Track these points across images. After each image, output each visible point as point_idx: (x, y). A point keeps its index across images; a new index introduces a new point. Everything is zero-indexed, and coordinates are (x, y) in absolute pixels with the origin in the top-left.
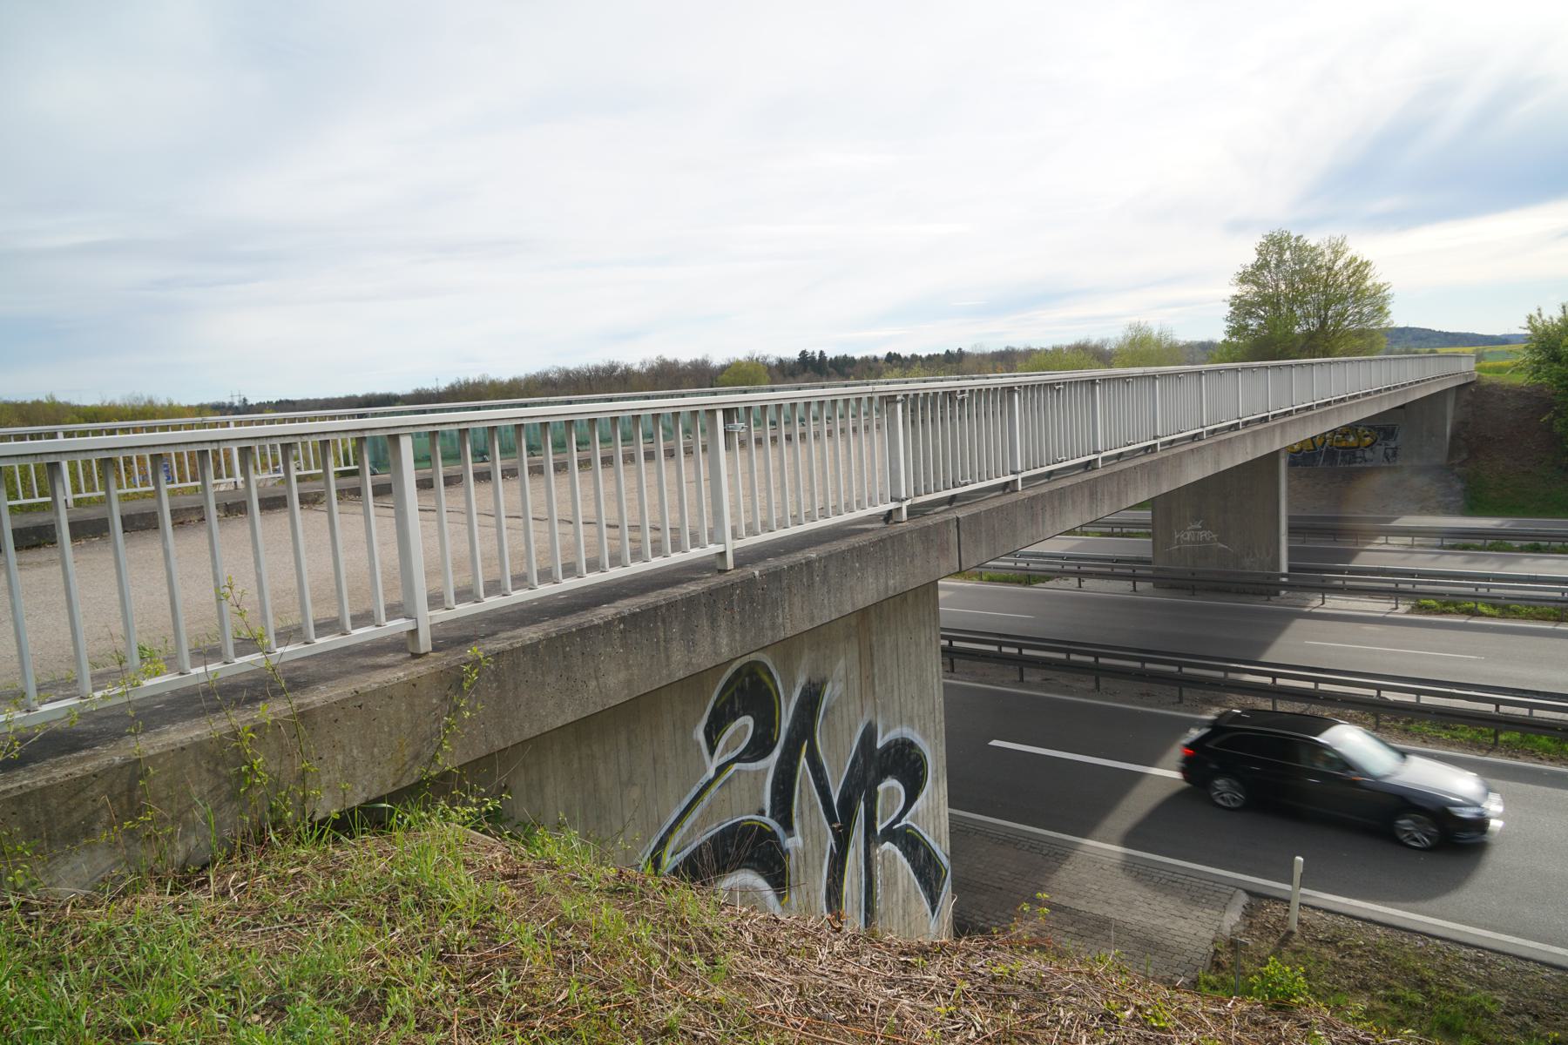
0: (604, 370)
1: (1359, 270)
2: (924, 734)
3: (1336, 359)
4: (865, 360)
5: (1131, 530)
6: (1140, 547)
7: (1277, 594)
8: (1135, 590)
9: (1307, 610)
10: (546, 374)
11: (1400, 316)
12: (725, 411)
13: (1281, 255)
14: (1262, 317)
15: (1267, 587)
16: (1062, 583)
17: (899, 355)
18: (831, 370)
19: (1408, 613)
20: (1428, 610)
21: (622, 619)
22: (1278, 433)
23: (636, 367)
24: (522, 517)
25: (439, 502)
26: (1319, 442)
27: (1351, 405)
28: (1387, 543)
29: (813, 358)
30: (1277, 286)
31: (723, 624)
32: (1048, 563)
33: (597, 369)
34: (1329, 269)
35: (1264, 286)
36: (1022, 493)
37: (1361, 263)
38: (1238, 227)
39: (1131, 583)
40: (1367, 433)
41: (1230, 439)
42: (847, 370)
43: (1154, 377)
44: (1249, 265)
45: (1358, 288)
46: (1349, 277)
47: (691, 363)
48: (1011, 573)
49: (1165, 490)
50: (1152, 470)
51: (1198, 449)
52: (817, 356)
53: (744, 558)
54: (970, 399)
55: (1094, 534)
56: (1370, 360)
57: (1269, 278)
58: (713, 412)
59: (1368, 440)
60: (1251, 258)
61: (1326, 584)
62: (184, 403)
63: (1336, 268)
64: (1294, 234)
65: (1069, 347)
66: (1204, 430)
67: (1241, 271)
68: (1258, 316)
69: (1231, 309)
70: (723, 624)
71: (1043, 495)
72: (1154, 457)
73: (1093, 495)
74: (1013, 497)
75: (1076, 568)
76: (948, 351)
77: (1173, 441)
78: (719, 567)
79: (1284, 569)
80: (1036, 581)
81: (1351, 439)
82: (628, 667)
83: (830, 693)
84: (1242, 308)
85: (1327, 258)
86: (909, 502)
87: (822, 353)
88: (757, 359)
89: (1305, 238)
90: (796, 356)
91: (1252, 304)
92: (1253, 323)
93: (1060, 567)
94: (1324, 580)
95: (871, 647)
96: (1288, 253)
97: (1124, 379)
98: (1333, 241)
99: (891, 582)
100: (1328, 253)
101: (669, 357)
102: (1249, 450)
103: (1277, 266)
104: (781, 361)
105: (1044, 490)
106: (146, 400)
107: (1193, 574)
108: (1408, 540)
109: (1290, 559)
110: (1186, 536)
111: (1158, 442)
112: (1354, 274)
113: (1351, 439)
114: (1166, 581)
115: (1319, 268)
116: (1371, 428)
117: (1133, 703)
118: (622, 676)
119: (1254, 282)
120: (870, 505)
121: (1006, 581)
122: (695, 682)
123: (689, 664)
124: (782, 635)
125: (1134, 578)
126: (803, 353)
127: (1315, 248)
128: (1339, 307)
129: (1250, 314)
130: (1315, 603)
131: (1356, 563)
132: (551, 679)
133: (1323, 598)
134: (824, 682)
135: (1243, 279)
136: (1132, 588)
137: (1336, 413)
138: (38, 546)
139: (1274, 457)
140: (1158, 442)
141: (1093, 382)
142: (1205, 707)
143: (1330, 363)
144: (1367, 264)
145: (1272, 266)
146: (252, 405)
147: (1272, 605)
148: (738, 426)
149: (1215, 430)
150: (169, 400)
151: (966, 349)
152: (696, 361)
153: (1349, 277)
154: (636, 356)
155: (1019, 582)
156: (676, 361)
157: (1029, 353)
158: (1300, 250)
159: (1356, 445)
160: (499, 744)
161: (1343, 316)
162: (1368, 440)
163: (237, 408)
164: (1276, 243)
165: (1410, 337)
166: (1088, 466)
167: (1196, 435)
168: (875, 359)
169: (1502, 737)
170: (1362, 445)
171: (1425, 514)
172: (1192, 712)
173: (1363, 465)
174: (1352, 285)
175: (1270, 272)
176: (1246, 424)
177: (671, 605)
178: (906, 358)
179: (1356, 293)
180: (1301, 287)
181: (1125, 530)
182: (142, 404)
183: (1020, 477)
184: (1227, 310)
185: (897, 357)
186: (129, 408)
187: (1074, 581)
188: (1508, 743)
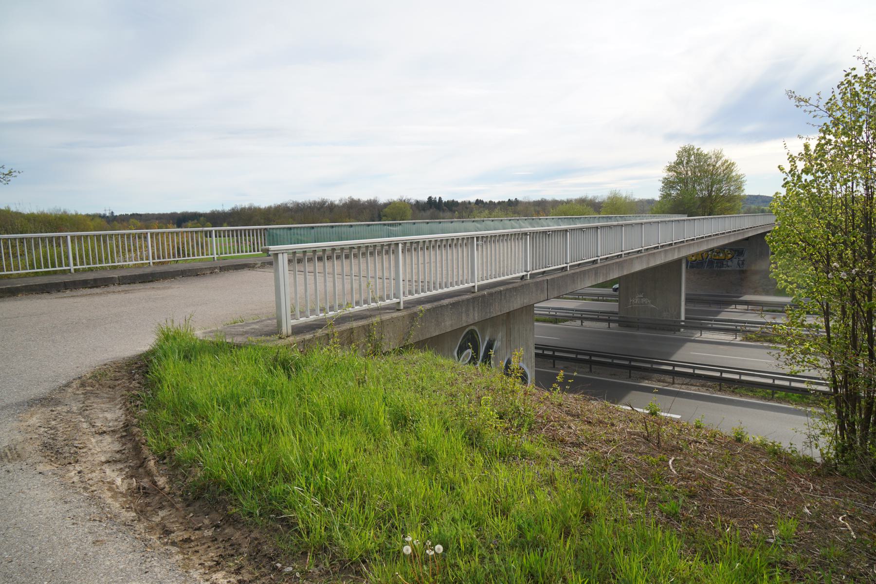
0: (319, 203)
1: (729, 166)
2: (528, 367)
3: (715, 216)
4: (464, 203)
5: (608, 298)
6: (613, 306)
7: (679, 331)
8: (609, 327)
9: (693, 338)
10: (286, 204)
11: (750, 189)
12: (477, 237)
13: (689, 158)
14: (679, 190)
15: (674, 326)
16: (573, 323)
17: (483, 201)
18: (445, 208)
19: (741, 341)
20: (750, 340)
21: (451, 304)
22: (676, 251)
23: (337, 202)
24: (351, 275)
25: (305, 269)
26: (705, 256)
27: (714, 239)
28: (735, 308)
29: (435, 201)
30: (687, 174)
31: (476, 309)
32: (566, 313)
33: (315, 203)
34: (714, 166)
35: (680, 173)
36: (569, 271)
37: (730, 163)
38: (671, 137)
39: (607, 324)
40: (729, 252)
41: (654, 253)
42: (454, 208)
43: (622, 225)
44: (672, 162)
45: (728, 177)
46: (724, 170)
47: (367, 201)
48: (548, 317)
49: (625, 273)
50: (620, 265)
51: (640, 257)
52: (437, 200)
53: (482, 288)
54: (552, 234)
55: (589, 300)
56: (725, 217)
57: (683, 169)
58: (473, 237)
59: (730, 255)
60: (674, 159)
61: (703, 326)
62: (83, 211)
63: (717, 165)
64: (696, 147)
65: (576, 200)
66: (643, 249)
67: (668, 165)
68: (677, 189)
69: (663, 184)
70: (476, 309)
71: (577, 272)
72: (621, 259)
73: (596, 274)
74: (566, 273)
75: (580, 315)
76: (509, 200)
77: (629, 253)
78: (473, 291)
79: (683, 318)
80: (560, 322)
81: (721, 255)
82: (452, 320)
83: (497, 344)
84: (668, 184)
85: (713, 160)
86: (530, 272)
87: (440, 198)
88: (404, 201)
89: (702, 149)
90: (425, 199)
91: (674, 183)
92: (674, 193)
93: (572, 315)
94: (701, 324)
95: (510, 329)
96: (693, 157)
97: (610, 226)
98: (716, 151)
99: (525, 301)
100: (713, 157)
101: (356, 198)
102: (663, 258)
103: (687, 163)
104: (417, 202)
105: (578, 270)
106: (62, 211)
107: (638, 320)
108: (746, 307)
109: (686, 313)
110: (635, 301)
111: (623, 253)
112: (726, 169)
113: (721, 255)
114: (625, 323)
115: (709, 165)
116: (731, 250)
117: (607, 377)
118: (450, 323)
119: (675, 171)
120: (422, 291)
121: (544, 321)
122: (454, 333)
123: (467, 322)
124: (492, 316)
125: (609, 321)
126: (430, 198)
127: (707, 155)
128: (718, 186)
129: (672, 187)
130: (697, 335)
131: (721, 317)
132: (433, 321)
133: (701, 333)
134: (494, 341)
135: (670, 169)
136: (608, 326)
137: (706, 243)
138: (152, 281)
139: (678, 262)
140: (623, 253)
141: (597, 228)
142: (642, 380)
143: (704, 219)
144: (733, 164)
145: (685, 163)
146: (117, 216)
147: (677, 336)
148: (480, 242)
149: (648, 249)
150: (76, 211)
151: (520, 199)
152: (370, 200)
153: (724, 170)
154: (337, 196)
155: (551, 322)
156: (359, 200)
157: (555, 203)
158: (699, 156)
159: (723, 258)
160: (421, 339)
161: (720, 190)
162: (730, 256)
163: (108, 217)
164: (687, 152)
165: (760, 200)
166: (595, 262)
167: (639, 251)
168: (469, 202)
169: (776, 395)
170: (727, 258)
171: (757, 295)
172: (635, 382)
173: (726, 269)
174: (725, 174)
175: (683, 166)
176: (662, 246)
177: (463, 301)
178: (486, 203)
179: (727, 178)
180: (699, 174)
181: (605, 298)
182: (60, 213)
183: (568, 265)
184: (661, 185)
185: (481, 202)
186: (53, 215)
187: (579, 322)
188: (778, 398)
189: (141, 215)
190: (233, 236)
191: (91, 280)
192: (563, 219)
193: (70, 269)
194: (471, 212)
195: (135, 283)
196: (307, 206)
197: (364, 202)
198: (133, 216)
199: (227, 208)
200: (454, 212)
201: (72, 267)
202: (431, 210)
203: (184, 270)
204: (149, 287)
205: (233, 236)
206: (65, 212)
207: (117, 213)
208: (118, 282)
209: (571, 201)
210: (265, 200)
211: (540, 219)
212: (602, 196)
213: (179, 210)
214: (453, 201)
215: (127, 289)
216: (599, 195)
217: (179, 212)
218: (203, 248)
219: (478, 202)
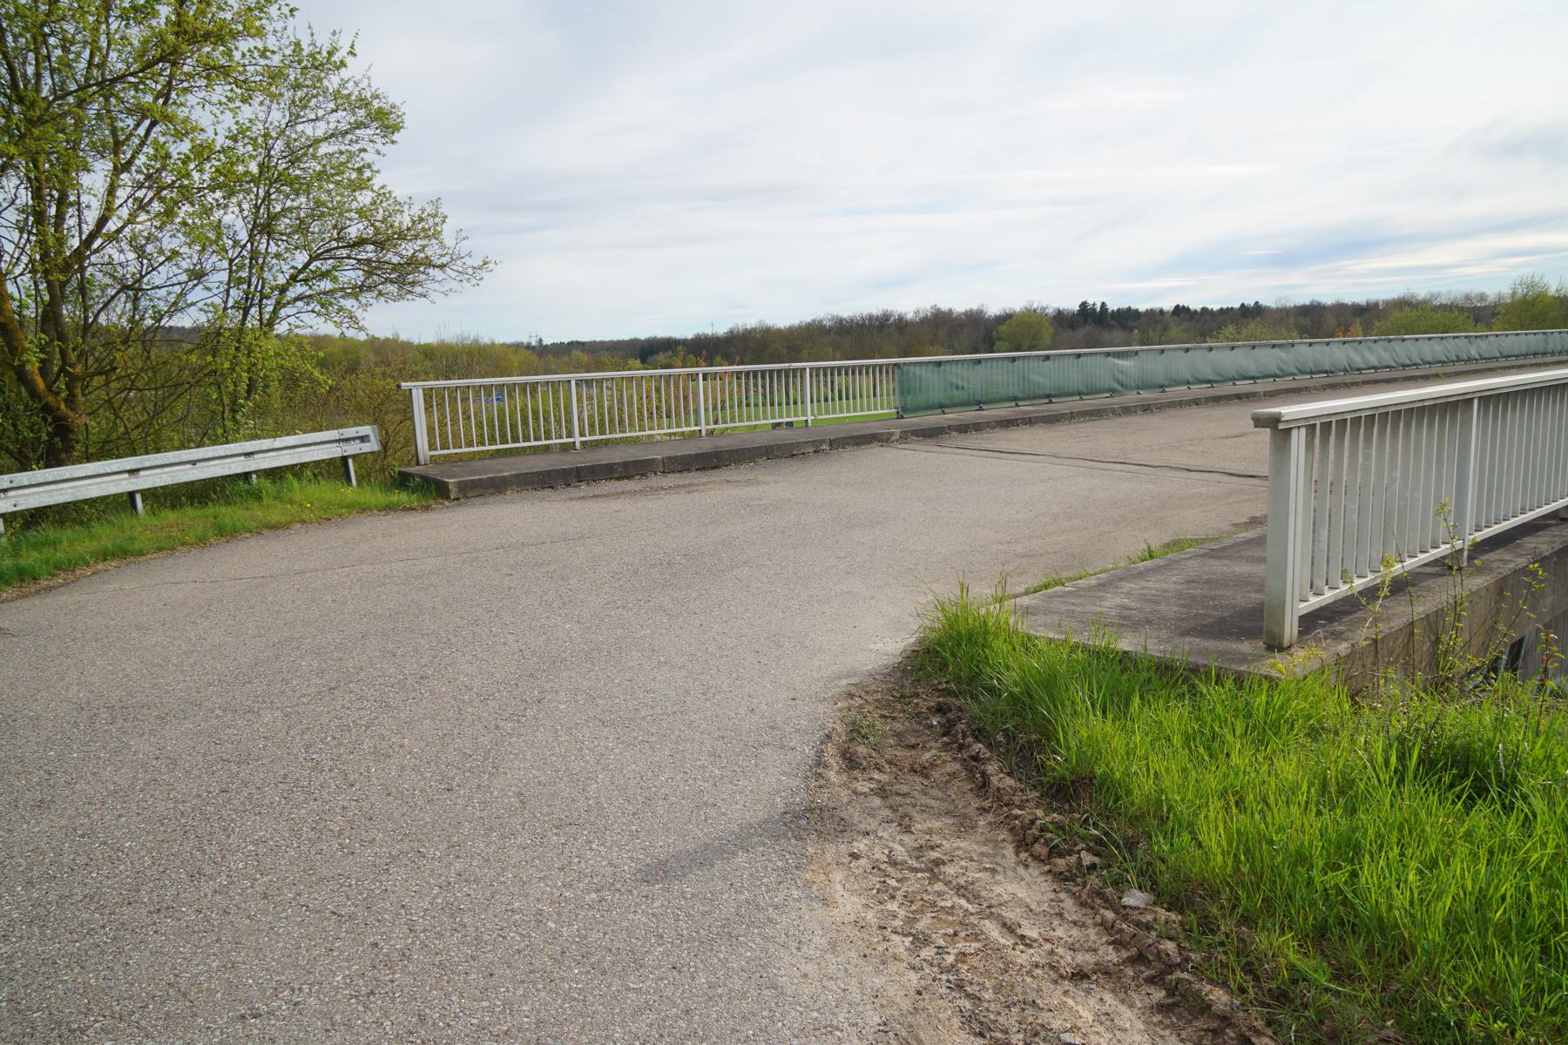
10: (820, 322)
17: (1188, 309)
18: (1113, 322)
23: (910, 316)
29: (1094, 310)
33: (871, 317)
47: (966, 313)
87: (1103, 304)
101: (944, 307)
106: (472, 338)
126: (1084, 304)
151: (1263, 302)
152: (971, 310)
154: (910, 303)
168: (1162, 312)
178: (1195, 311)
182: (469, 342)
189: (583, 344)
190: (867, 373)
191: (619, 464)
192: (1472, 339)
193: (574, 443)
194: (1165, 329)
195: (689, 470)
196: (857, 323)
197: (959, 315)
198: (571, 344)
199: (721, 329)
200: (1132, 331)
201: (578, 439)
202: (1087, 327)
203: (770, 446)
204: (717, 479)
205: (867, 373)
206: (476, 341)
207: (547, 342)
208: (661, 469)
209: (1376, 304)
210: (785, 313)
211: (1404, 340)
212: (1449, 292)
213: (643, 334)
214: (1129, 309)
215: (687, 482)
216: (1444, 290)
217: (643, 337)
218: (684, 407)
219: (1180, 311)
